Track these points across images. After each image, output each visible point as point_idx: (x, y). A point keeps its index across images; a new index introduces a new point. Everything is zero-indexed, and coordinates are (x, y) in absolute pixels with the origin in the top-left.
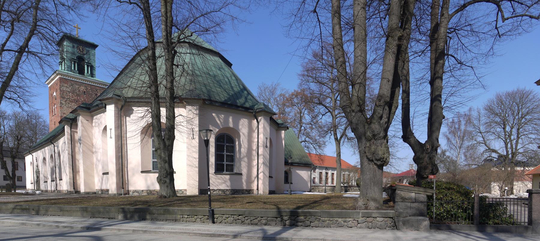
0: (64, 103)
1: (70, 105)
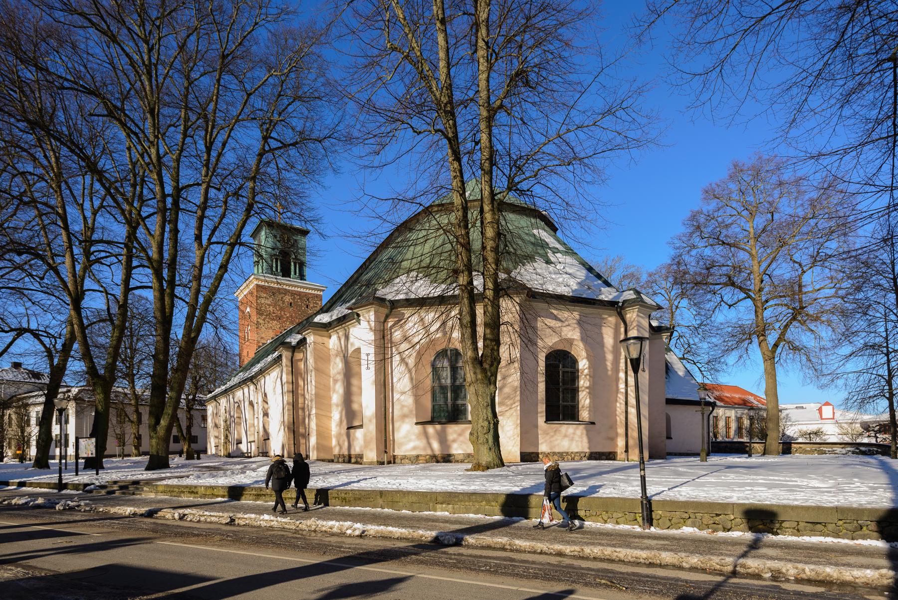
0: (261, 321)
1: (270, 325)
